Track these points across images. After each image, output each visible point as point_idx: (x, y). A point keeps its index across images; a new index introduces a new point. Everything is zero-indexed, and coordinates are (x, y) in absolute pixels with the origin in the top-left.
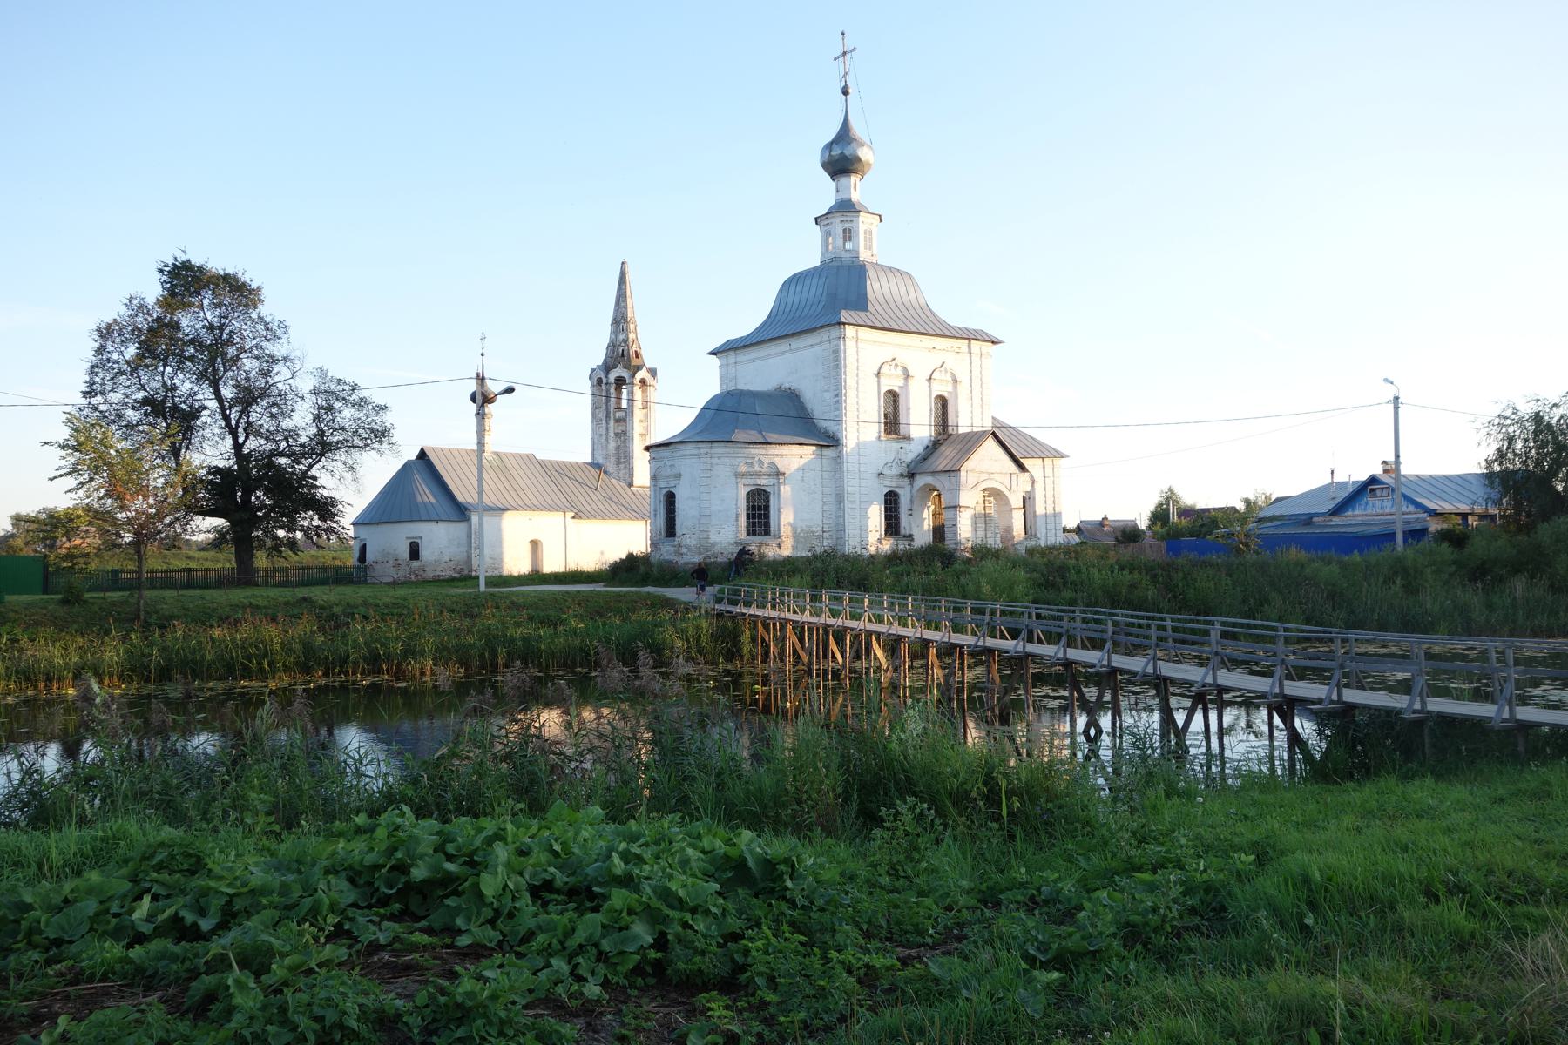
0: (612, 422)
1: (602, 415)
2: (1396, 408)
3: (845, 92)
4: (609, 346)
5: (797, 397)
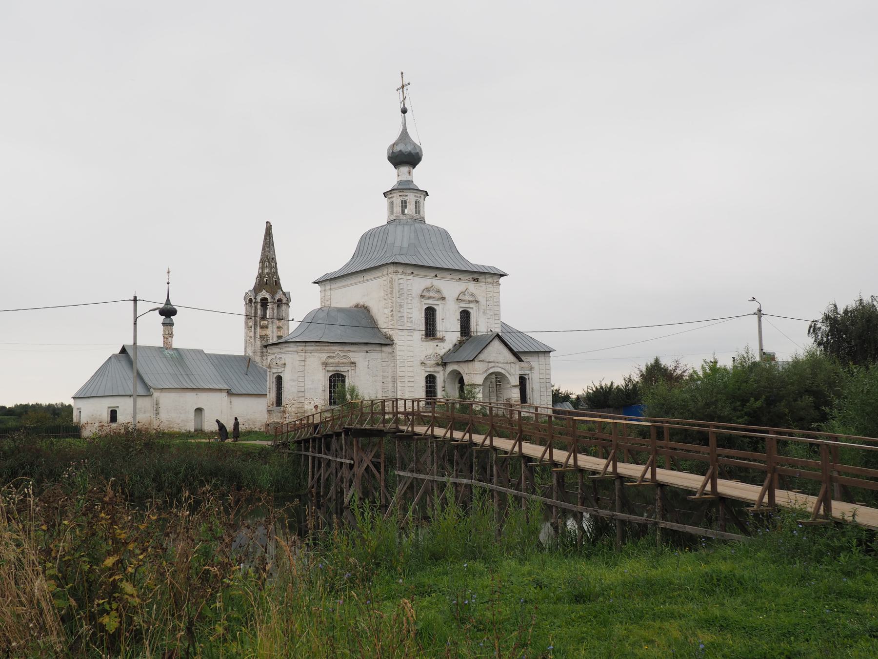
0: (258, 329)
1: (251, 323)
2: (760, 318)
3: (404, 111)
4: (258, 277)
5: (368, 311)
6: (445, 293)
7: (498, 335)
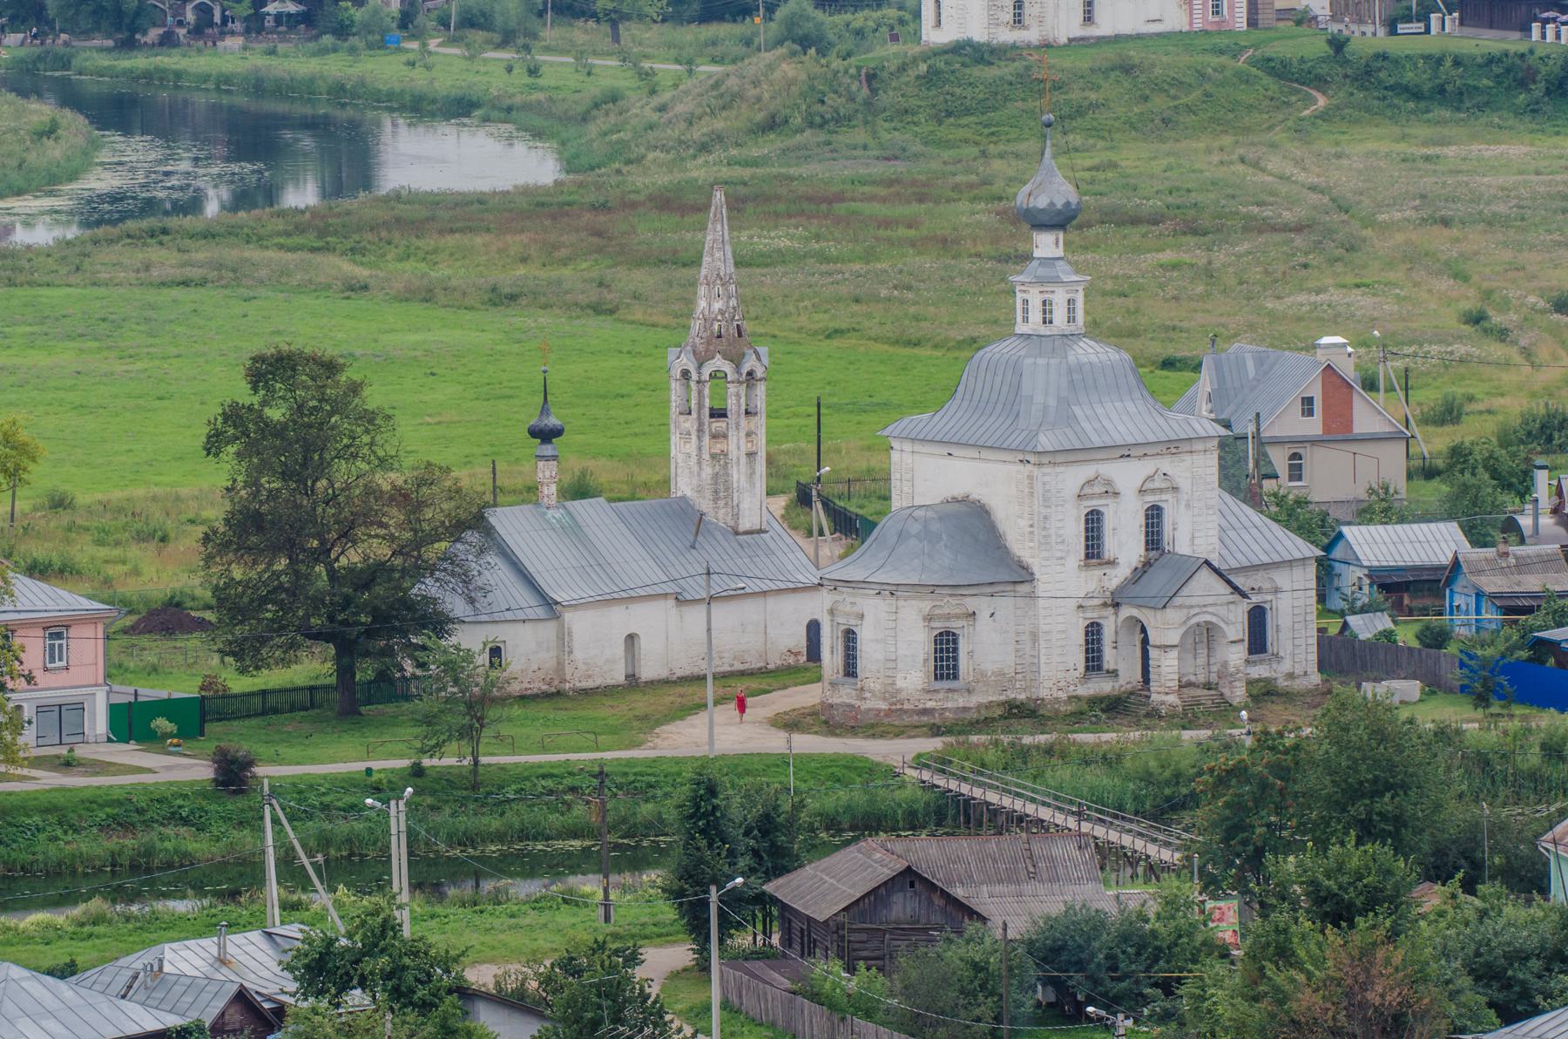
5: (988, 513)
7: (1207, 562)
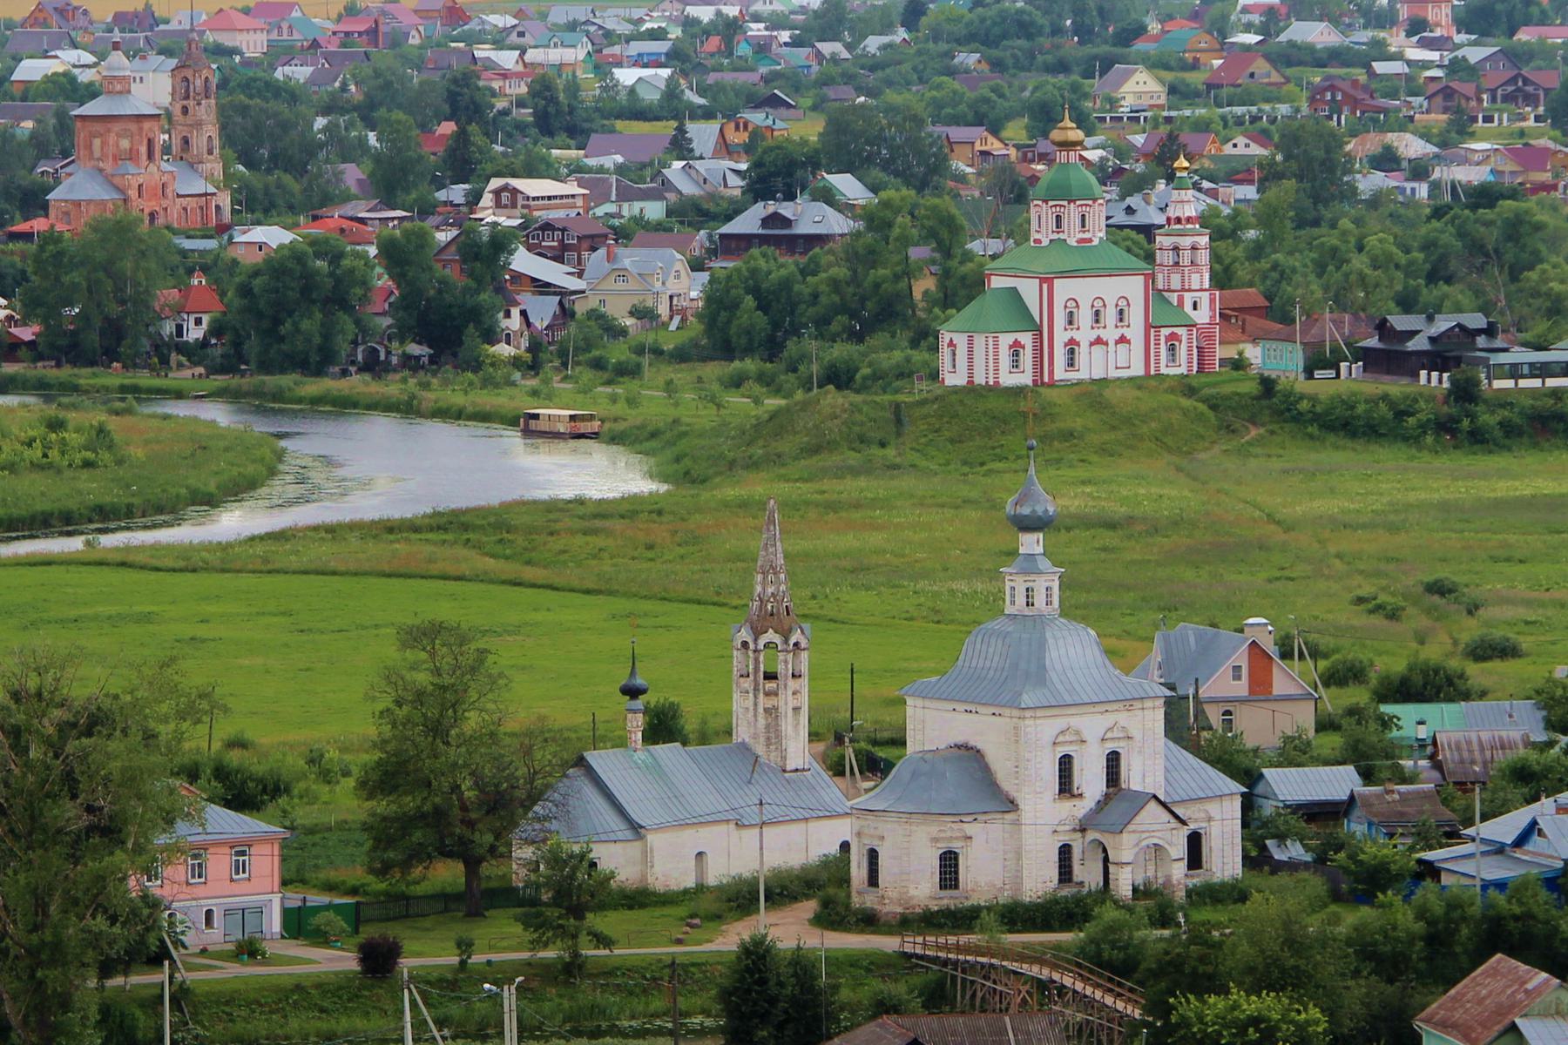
0: (761, 695)
6: (1086, 736)
